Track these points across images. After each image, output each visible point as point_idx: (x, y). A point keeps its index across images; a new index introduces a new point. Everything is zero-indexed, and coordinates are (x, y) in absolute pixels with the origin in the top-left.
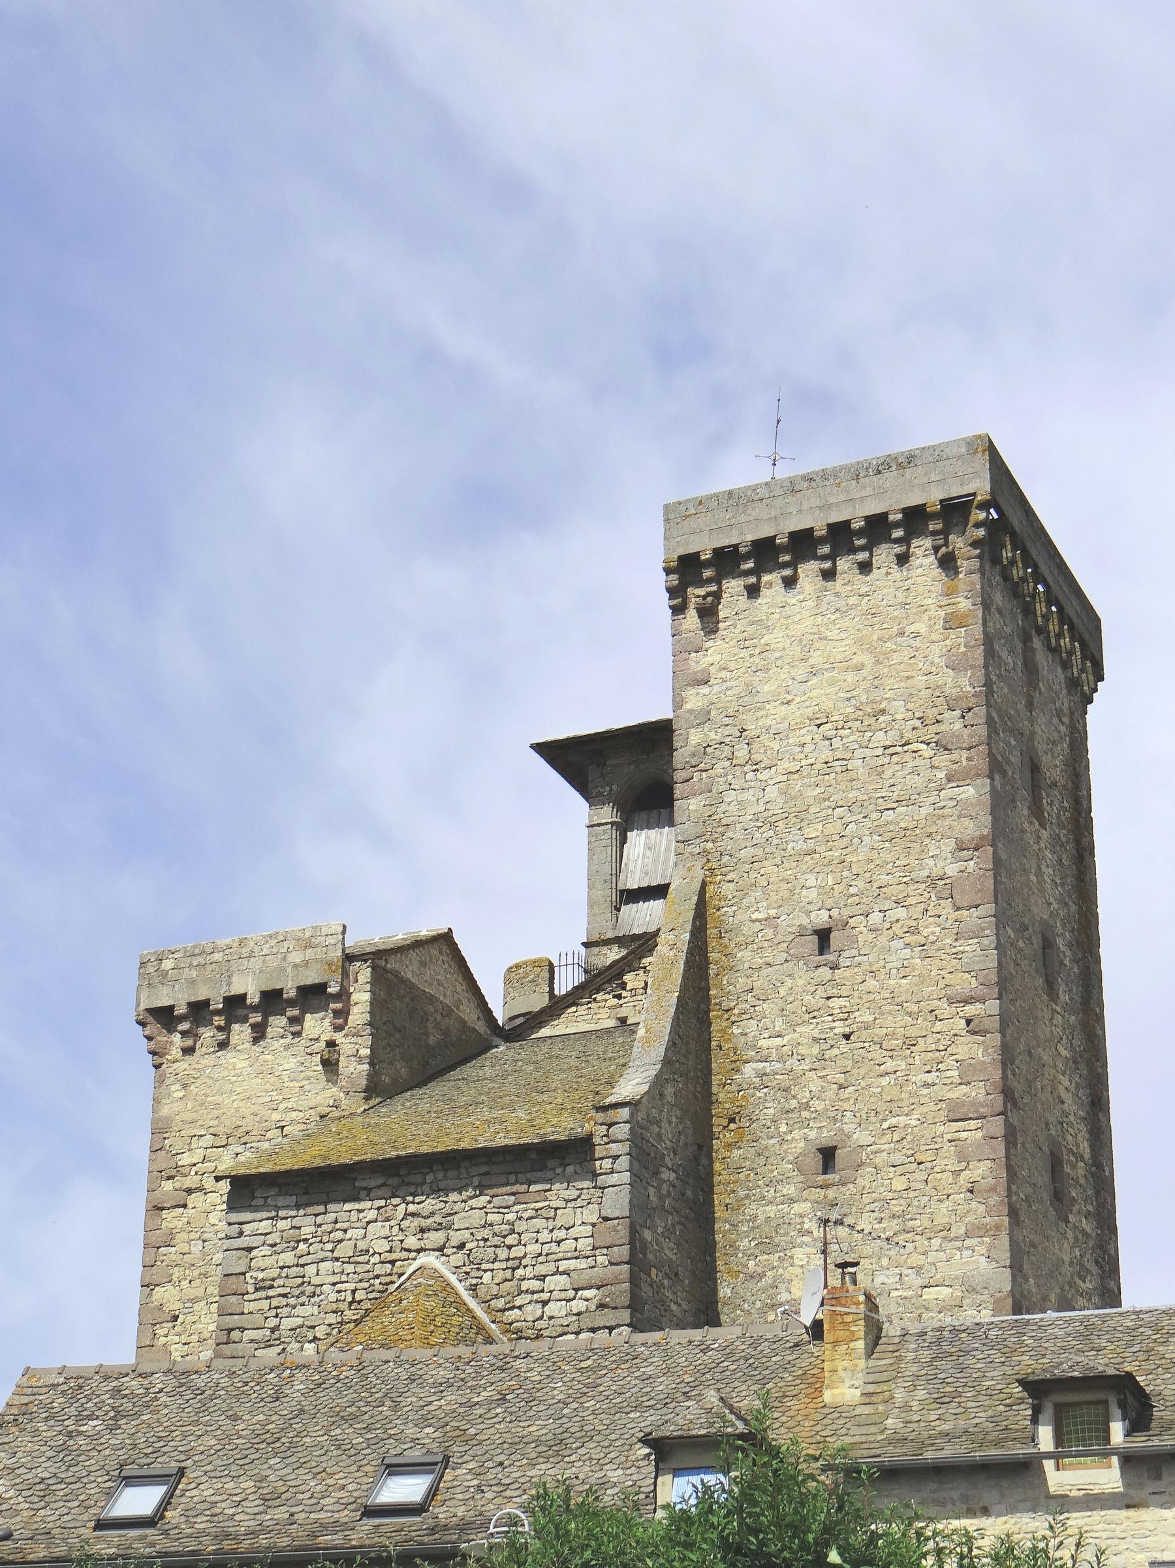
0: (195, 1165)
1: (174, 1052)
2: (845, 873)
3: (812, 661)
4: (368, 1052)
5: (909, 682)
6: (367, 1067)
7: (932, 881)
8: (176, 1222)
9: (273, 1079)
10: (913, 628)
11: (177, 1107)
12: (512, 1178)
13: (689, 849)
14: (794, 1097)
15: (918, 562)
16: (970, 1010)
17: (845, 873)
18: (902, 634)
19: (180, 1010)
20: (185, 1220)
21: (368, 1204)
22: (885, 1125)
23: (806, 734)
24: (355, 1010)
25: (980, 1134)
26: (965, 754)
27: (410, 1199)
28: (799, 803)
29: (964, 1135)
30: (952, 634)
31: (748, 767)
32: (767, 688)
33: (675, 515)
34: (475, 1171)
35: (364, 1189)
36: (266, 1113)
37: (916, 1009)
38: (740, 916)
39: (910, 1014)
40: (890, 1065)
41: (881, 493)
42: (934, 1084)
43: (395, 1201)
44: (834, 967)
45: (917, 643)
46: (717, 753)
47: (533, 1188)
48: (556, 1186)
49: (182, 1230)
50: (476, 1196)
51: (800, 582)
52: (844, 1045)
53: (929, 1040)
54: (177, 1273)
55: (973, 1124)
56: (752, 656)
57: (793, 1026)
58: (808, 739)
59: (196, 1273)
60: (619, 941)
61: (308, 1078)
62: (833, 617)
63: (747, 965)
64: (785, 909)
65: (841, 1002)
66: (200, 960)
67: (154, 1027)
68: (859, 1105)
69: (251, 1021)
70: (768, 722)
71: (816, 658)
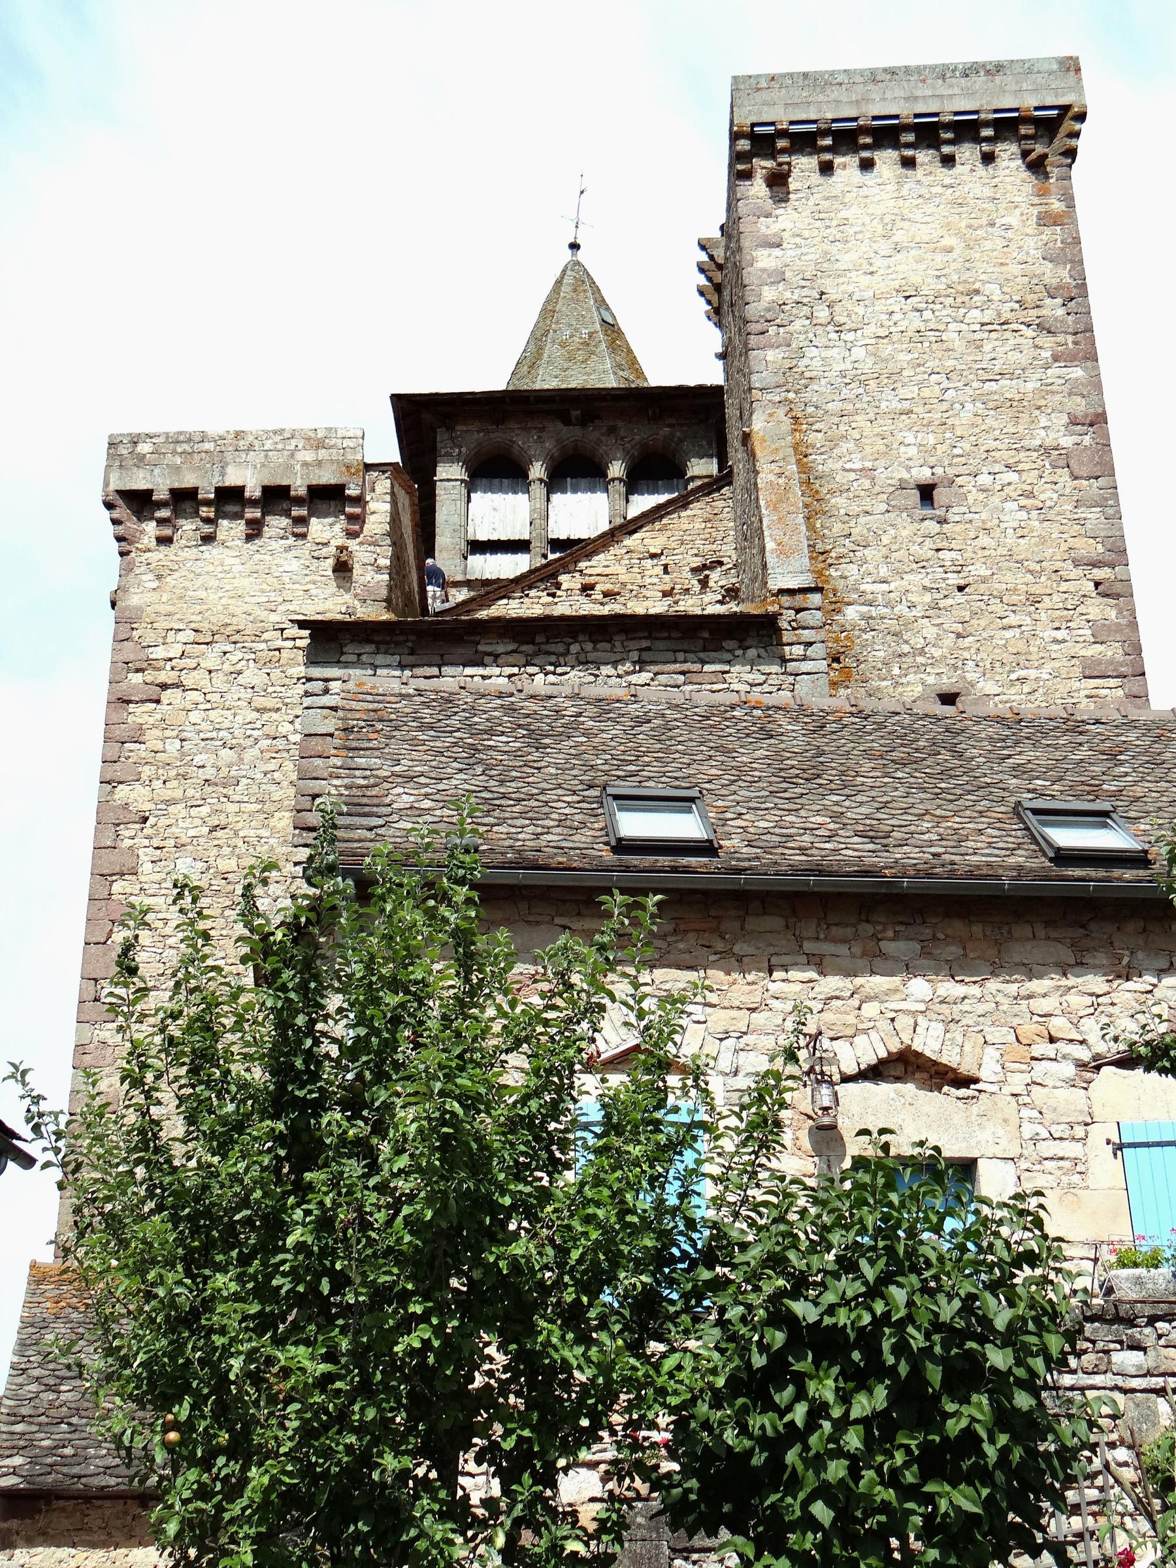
0: (170, 659)
1: (146, 541)
2: (948, 435)
3: (895, 239)
4: (388, 562)
5: (1003, 269)
6: (386, 577)
7: (1045, 450)
8: (146, 717)
9: (270, 579)
10: (1003, 221)
11: (150, 597)
12: (681, 656)
13: (769, 397)
14: (906, 642)
15: (1005, 164)
16: (1100, 574)
17: (948, 435)
18: (992, 225)
19: (161, 494)
20: (159, 717)
21: (497, 671)
22: (1013, 676)
23: (896, 303)
24: (371, 519)
25: (1120, 692)
26: (1070, 338)
27: (551, 668)
28: (891, 365)
29: (1103, 692)
30: (1048, 231)
31: (830, 328)
32: (847, 257)
33: (741, 87)
34: (632, 645)
35: (489, 654)
36: (264, 615)
37: (1038, 568)
38: (830, 464)
39: (1031, 572)
40: (1013, 620)
41: (969, 93)
42: (1064, 641)
43: (531, 670)
44: (942, 521)
45: (1010, 234)
46: (794, 311)
47: (707, 668)
48: (737, 668)
49: (154, 726)
50: (634, 672)
51: (877, 167)
52: (960, 598)
53: (1056, 597)
54: (147, 771)
55: (1112, 682)
56: (828, 227)
57: (900, 574)
58: (896, 308)
59: (173, 773)
60: (468, 584)
61: (314, 583)
62: (916, 202)
63: (842, 512)
64: (881, 463)
65: (953, 554)
66: (186, 447)
67: (122, 512)
68: (983, 655)
69: (248, 515)
70: (851, 288)
71: (899, 236)
